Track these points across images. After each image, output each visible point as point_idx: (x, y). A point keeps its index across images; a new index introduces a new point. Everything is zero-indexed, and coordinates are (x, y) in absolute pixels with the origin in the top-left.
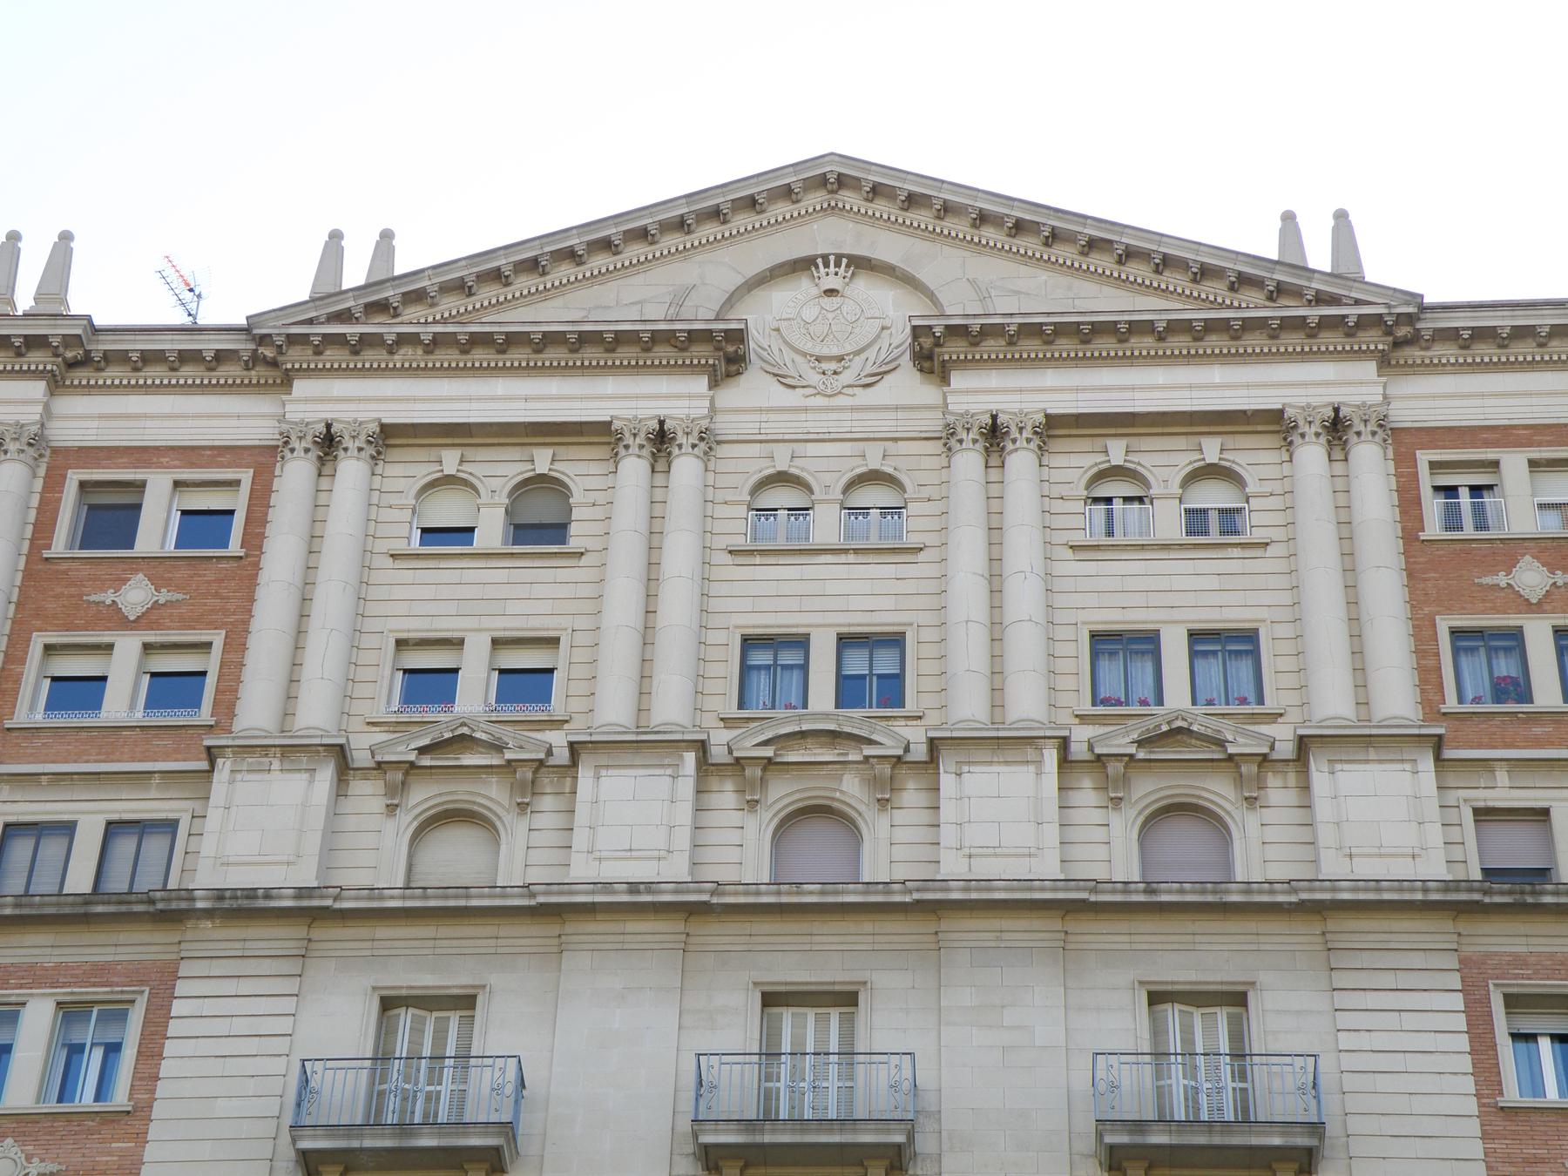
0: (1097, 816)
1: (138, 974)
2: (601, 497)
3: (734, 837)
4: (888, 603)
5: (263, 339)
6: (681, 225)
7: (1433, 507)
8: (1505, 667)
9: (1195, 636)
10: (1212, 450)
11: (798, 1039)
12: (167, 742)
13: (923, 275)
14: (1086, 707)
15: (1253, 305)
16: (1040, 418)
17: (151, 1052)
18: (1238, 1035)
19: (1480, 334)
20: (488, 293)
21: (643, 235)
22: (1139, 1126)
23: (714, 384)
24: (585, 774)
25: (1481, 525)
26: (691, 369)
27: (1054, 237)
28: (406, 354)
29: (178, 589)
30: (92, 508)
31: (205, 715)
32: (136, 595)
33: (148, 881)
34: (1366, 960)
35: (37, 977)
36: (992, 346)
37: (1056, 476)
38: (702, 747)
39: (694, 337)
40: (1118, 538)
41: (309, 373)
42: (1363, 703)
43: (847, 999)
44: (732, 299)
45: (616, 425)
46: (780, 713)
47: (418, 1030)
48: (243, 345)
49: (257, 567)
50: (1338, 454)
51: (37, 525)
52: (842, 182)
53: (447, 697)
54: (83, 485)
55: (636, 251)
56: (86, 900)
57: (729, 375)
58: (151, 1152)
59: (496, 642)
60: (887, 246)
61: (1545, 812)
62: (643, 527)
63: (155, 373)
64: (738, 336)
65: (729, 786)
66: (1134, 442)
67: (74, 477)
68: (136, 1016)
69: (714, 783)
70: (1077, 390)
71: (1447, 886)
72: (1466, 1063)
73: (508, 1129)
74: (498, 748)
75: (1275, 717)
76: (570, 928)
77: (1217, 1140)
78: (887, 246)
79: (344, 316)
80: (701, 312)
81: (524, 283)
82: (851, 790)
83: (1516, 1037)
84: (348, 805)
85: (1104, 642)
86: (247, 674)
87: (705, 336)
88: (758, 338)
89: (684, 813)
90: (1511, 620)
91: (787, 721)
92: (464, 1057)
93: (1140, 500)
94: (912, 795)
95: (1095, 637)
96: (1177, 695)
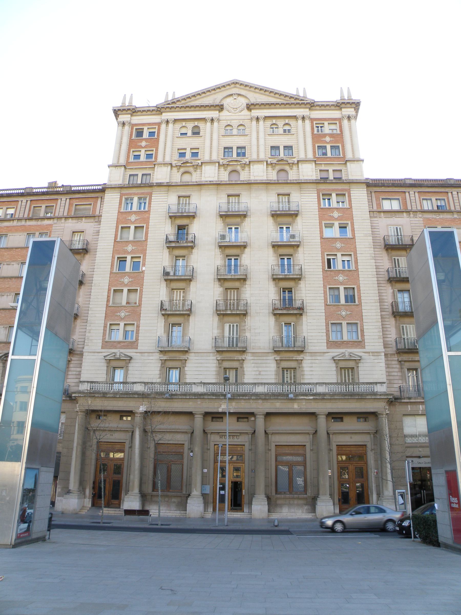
0: (271, 171)
1: (147, 194)
2: (204, 128)
3: (223, 174)
4: (243, 142)
5: (158, 108)
6: (214, 90)
7: (316, 129)
8: (324, 151)
9: (284, 147)
10: (287, 121)
11: (232, 201)
12: (149, 163)
13: (248, 96)
14: (270, 157)
15: (292, 101)
16: (264, 117)
17: (150, 204)
18: (289, 199)
19: (322, 105)
20: (188, 100)
21: (209, 91)
22: (276, 211)
23: (219, 112)
24: (203, 166)
25: (322, 132)
26: (216, 110)
27: (266, 91)
28: (177, 109)
29: (149, 142)
30: (137, 132)
31: (153, 159)
32: (144, 144)
33: (148, 182)
34: (305, 190)
35: (135, 194)
36: (257, 106)
37: (266, 125)
38: (219, 162)
39: (216, 105)
40: (274, 133)
41: (164, 112)
42: (306, 156)
43: (238, 195)
44: (222, 100)
45: (206, 118)
46: (229, 158)
47: (183, 200)
48: (156, 109)
49: (159, 139)
50: (303, 122)
51: (130, 135)
52: (237, 83)
53: (185, 156)
54: (136, 129)
55: (208, 93)
56: (140, 184)
57: (221, 111)
58: (151, 216)
59: (191, 149)
60: (243, 92)
61: (328, 170)
62: (210, 133)
63: (144, 113)
64: (222, 105)
65: (222, 168)
66: (277, 120)
67: (135, 128)
68: (148, 199)
69: (220, 167)
70: (269, 112)
71: (316, 180)
72: (317, 202)
73: (195, 213)
74: (192, 163)
75: (294, 158)
76: (202, 187)
77: (286, 213)
78: (243, 92)
79: (169, 104)
80: (217, 102)
81: (193, 98)
82: (239, 168)
83: (323, 199)
84: (172, 171)
85: (272, 148)
86: (158, 154)
87: (218, 105)
88: (225, 106)
89: (217, 171)
90: (325, 145)
91: (230, 159)
92: (189, 204)
93: (277, 128)
94: (247, 168)
95: (271, 147)
96: (282, 155)
